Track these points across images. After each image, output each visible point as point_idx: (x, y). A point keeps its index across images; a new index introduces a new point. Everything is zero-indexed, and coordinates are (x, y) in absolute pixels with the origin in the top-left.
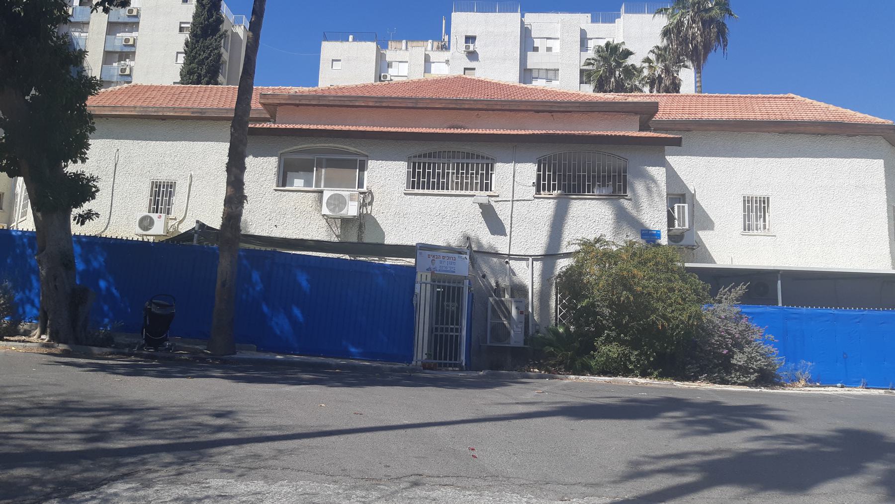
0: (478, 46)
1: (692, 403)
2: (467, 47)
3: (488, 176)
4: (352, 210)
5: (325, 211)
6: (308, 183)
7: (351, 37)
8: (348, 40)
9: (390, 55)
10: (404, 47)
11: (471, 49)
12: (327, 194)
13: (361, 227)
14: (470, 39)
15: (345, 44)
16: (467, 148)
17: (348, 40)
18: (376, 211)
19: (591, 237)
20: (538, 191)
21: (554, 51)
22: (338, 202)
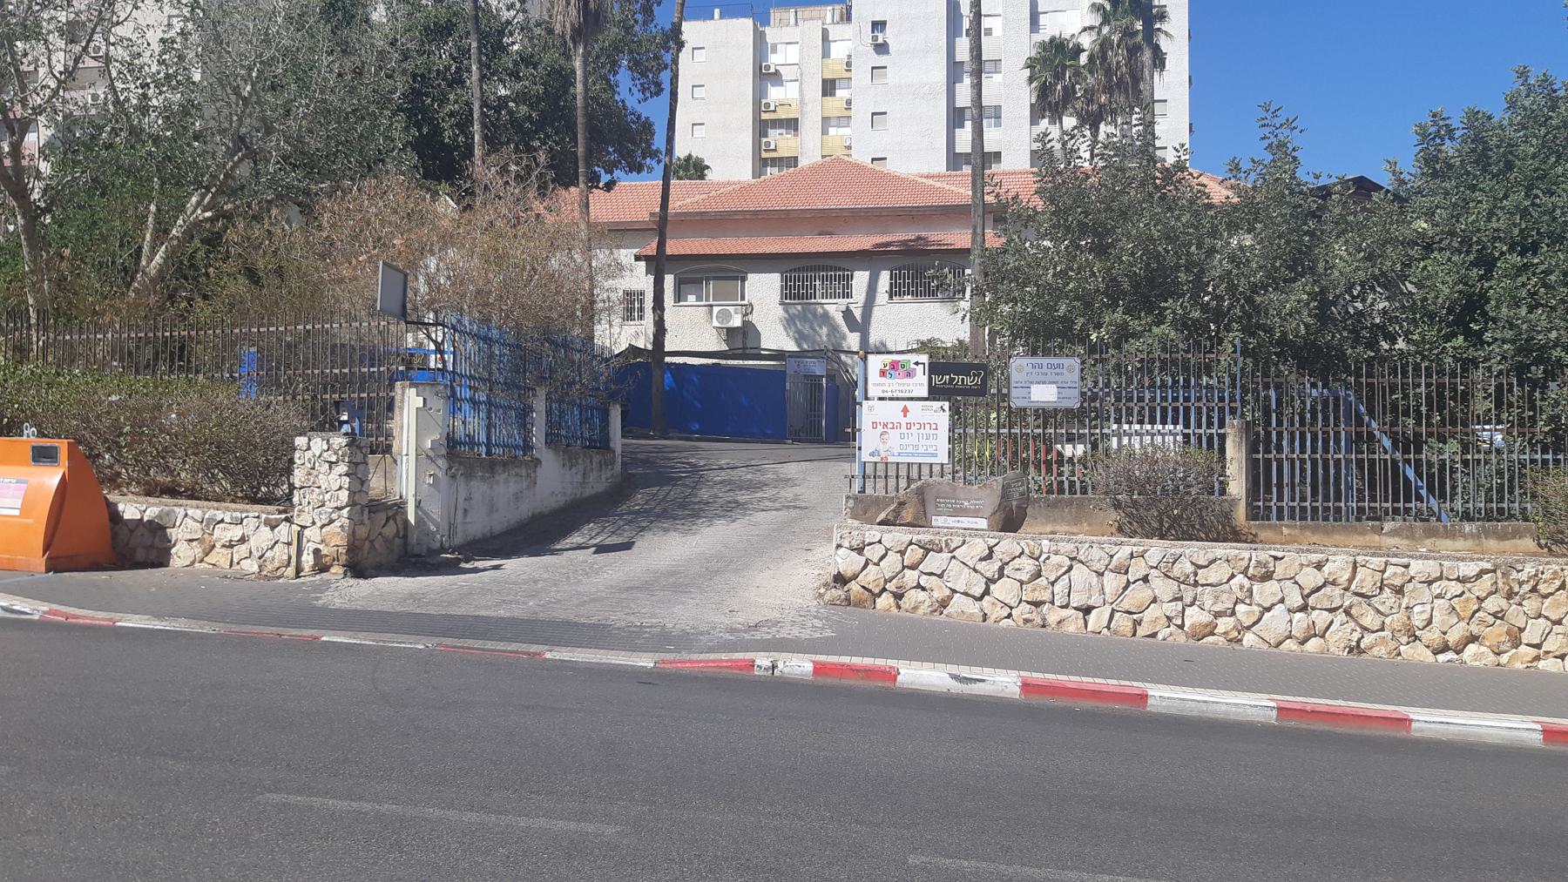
0: (889, 36)
1: (555, 513)
2: (875, 38)
3: (849, 286)
4: (737, 322)
5: (716, 323)
6: (699, 299)
7: (717, 11)
8: (712, 18)
9: (771, 34)
10: (792, 21)
11: (880, 41)
12: (716, 310)
13: (745, 334)
14: (878, 26)
15: (709, 23)
16: (831, 262)
17: (712, 18)
18: (753, 318)
19: (925, 339)
20: (891, 297)
21: (995, 33)
22: (725, 316)
